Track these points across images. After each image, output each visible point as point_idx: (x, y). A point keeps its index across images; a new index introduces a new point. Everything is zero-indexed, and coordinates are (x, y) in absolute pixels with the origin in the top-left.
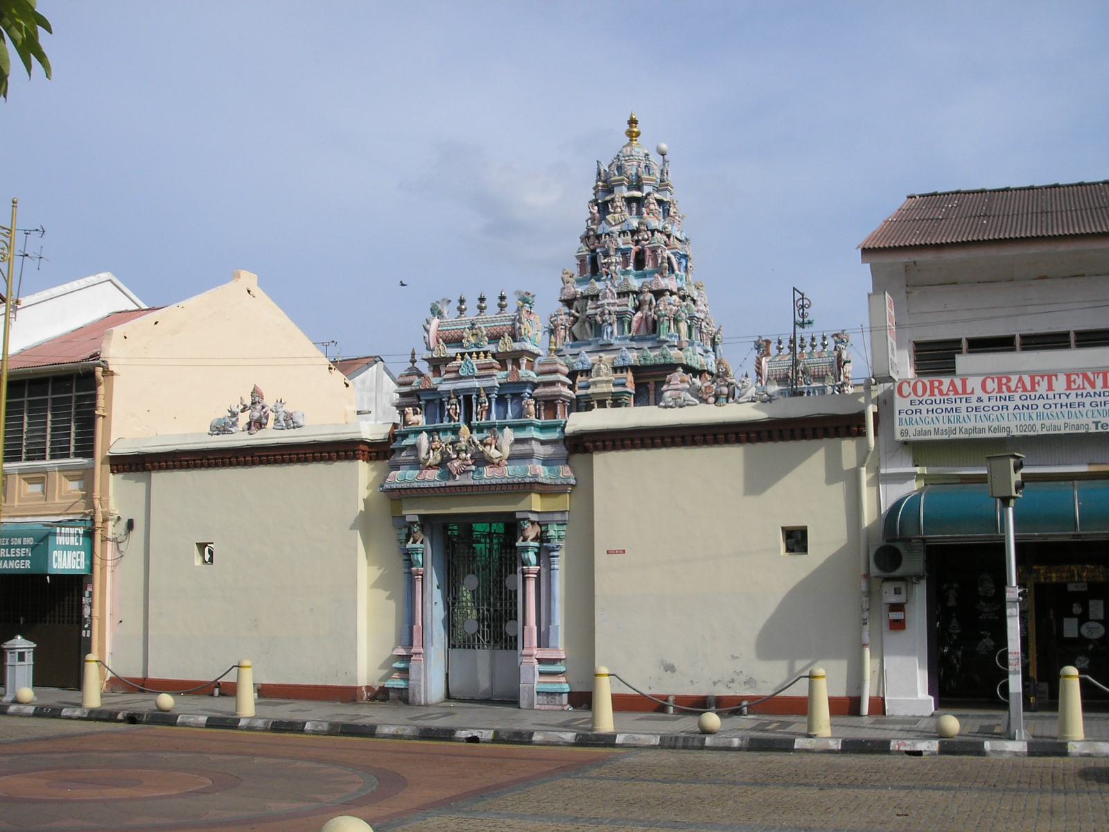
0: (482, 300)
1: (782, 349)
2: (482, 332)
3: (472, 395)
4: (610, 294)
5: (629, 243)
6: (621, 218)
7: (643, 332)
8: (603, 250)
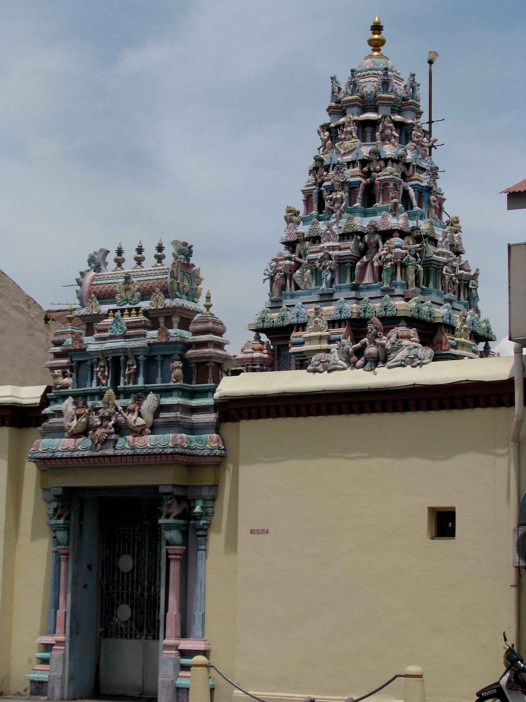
3: (120, 357)
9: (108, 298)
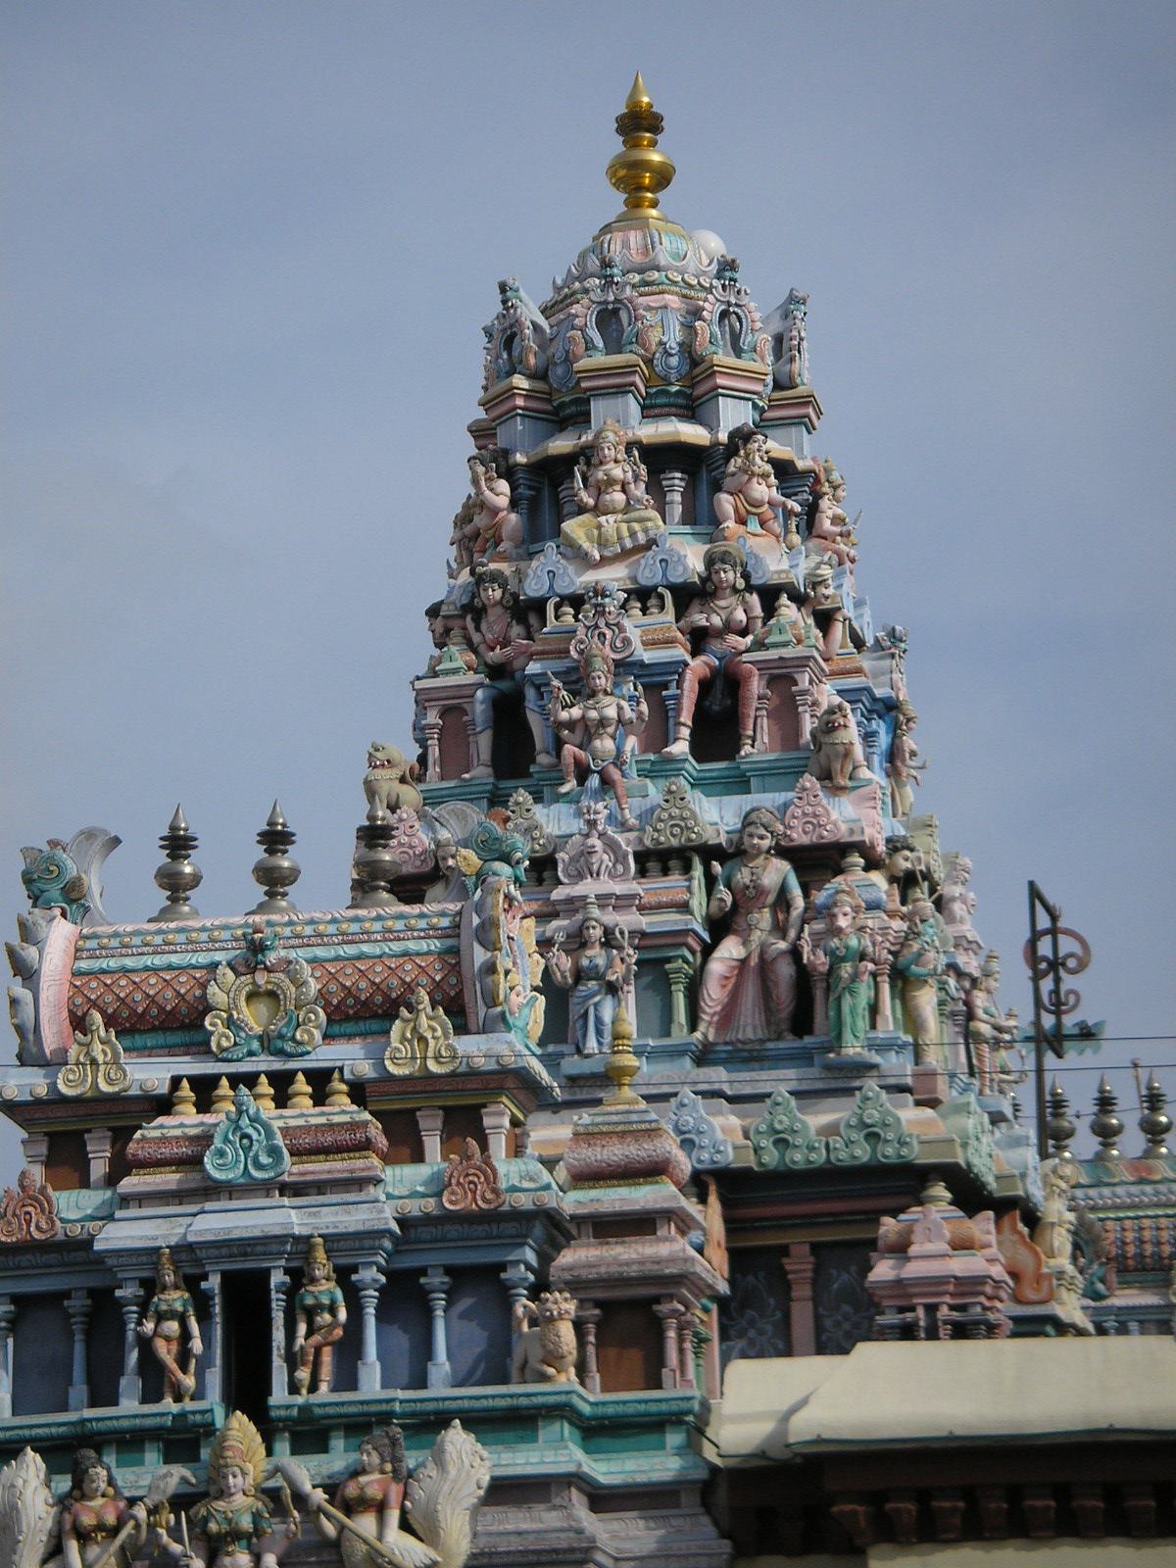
0: (275, 839)
1: (1167, 1128)
2: (300, 984)
4: (603, 858)
5: (670, 642)
6: (633, 534)
7: (749, 1026)
8: (559, 665)
9: (154, 1029)
